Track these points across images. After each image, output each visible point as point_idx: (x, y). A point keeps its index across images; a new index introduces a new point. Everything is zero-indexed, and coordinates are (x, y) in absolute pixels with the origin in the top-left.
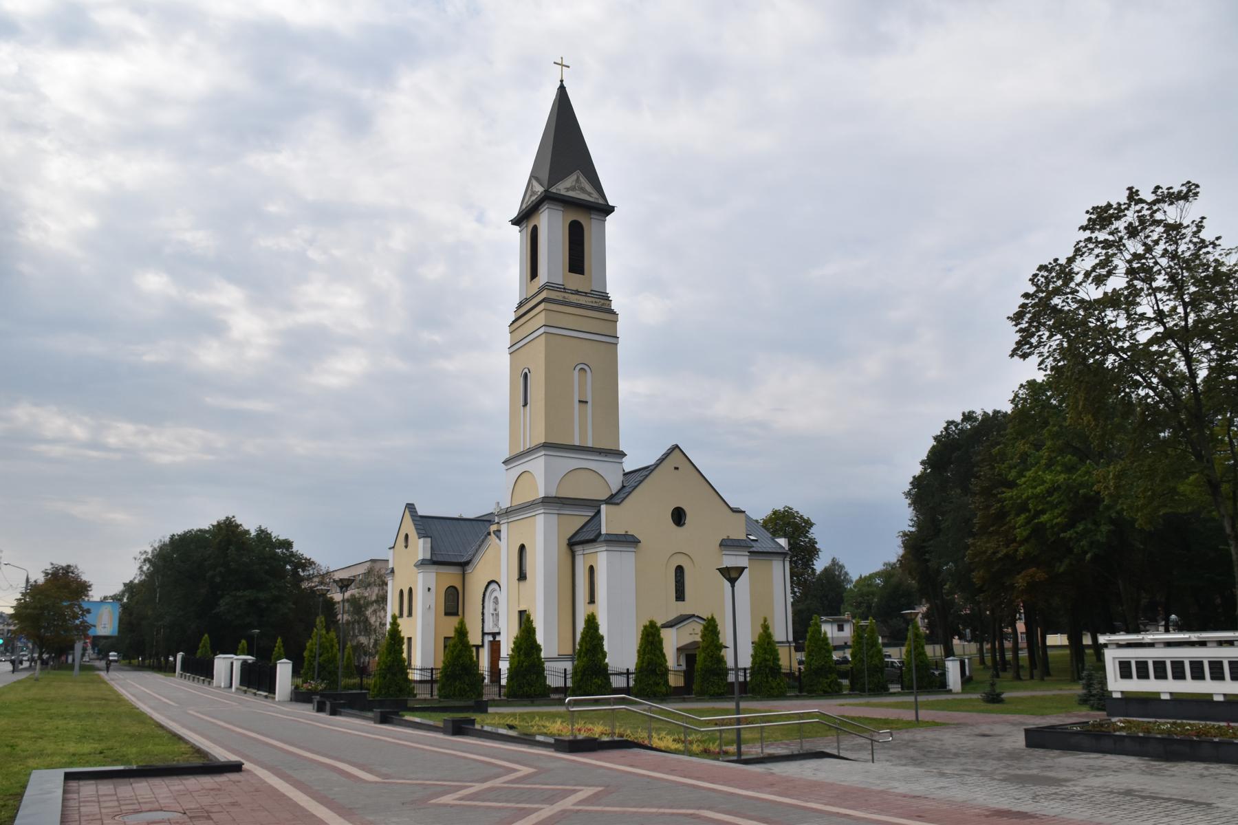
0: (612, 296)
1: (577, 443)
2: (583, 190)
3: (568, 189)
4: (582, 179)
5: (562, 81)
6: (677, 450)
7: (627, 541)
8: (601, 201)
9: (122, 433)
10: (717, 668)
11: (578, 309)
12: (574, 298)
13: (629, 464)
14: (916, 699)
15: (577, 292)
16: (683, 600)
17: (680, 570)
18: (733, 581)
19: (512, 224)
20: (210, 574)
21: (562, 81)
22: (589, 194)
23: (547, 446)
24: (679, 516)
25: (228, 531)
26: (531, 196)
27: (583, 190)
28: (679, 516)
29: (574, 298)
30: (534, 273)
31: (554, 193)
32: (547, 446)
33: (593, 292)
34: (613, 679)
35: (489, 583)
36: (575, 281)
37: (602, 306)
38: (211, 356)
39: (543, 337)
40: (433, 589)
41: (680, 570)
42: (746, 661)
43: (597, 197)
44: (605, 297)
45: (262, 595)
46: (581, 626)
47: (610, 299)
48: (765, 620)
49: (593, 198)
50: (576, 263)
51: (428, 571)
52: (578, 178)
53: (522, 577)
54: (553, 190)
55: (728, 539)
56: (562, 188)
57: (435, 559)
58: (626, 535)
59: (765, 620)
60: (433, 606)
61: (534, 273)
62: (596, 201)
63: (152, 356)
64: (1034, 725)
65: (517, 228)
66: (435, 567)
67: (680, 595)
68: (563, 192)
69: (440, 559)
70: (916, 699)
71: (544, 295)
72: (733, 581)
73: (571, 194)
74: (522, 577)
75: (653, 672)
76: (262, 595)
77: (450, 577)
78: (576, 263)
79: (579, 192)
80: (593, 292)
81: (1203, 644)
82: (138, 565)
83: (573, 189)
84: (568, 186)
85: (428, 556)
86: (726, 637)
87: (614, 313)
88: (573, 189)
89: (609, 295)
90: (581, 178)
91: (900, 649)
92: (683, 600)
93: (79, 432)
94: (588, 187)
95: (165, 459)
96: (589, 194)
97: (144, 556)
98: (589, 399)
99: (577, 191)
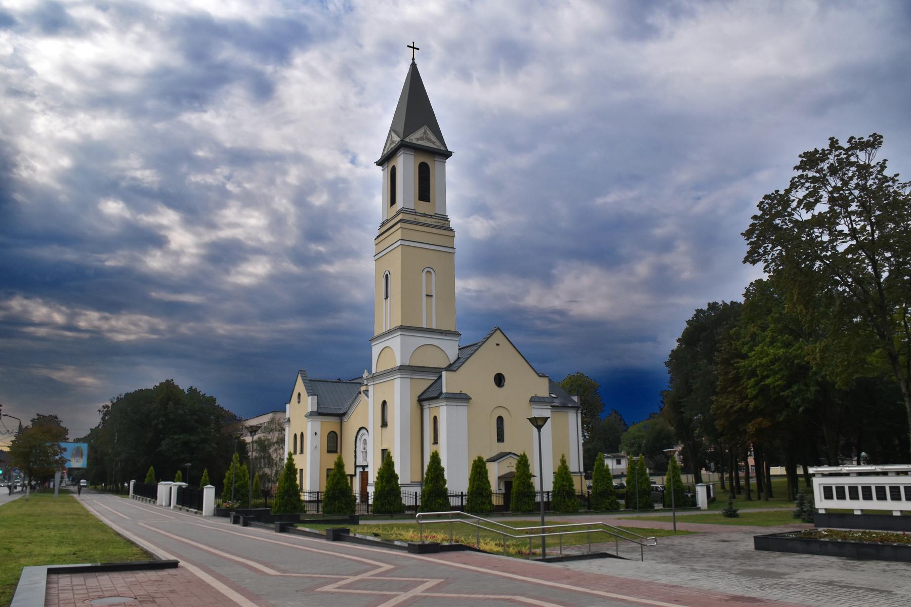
1: (425, 326)
2: (429, 140)
3: (418, 139)
4: (429, 132)
5: (413, 59)
6: (498, 332)
7: (461, 398)
8: (442, 148)
12: (422, 220)
14: (674, 514)
15: (425, 215)
16: (503, 441)
17: (500, 420)
18: (539, 428)
19: (377, 165)
20: (154, 422)
21: (413, 59)
22: (434, 143)
23: (402, 328)
24: (499, 380)
27: (429, 140)
28: (499, 380)
29: (422, 220)
30: (393, 201)
32: (402, 328)
33: (436, 215)
34: (451, 499)
36: (423, 207)
37: (442, 224)
38: (155, 262)
39: (400, 248)
40: (319, 433)
41: (500, 420)
42: (549, 486)
43: (440, 145)
44: (446, 219)
45: (193, 438)
46: (427, 460)
48: (563, 456)
49: (436, 145)
50: (424, 194)
51: (315, 420)
52: (425, 131)
53: (384, 424)
54: (407, 140)
55: (536, 397)
58: (460, 394)
59: (563, 456)
60: (319, 446)
61: (393, 201)
62: (439, 148)
63: (112, 262)
65: (380, 168)
66: (320, 417)
67: (500, 438)
68: (414, 141)
69: (324, 411)
70: (674, 514)
71: (400, 217)
72: (539, 428)
73: (420, 143)
74: (384, 424)
75: (481, 494)
76: (193, 438)
77: (331, 424)
78: (424, 194)
79: (426, 141)
80: (436, 215)
81: (885, 474)
83: (422, 139)
85: (315, 409)
86: (534, 469)
87: (451, 230)
88: (422, 139)
89: (448, 217)
92: (503, 441)
94: (433, 138)
95: (121, 337)
96: (434, 143)
98: (434, 294)
99: (425, 141)
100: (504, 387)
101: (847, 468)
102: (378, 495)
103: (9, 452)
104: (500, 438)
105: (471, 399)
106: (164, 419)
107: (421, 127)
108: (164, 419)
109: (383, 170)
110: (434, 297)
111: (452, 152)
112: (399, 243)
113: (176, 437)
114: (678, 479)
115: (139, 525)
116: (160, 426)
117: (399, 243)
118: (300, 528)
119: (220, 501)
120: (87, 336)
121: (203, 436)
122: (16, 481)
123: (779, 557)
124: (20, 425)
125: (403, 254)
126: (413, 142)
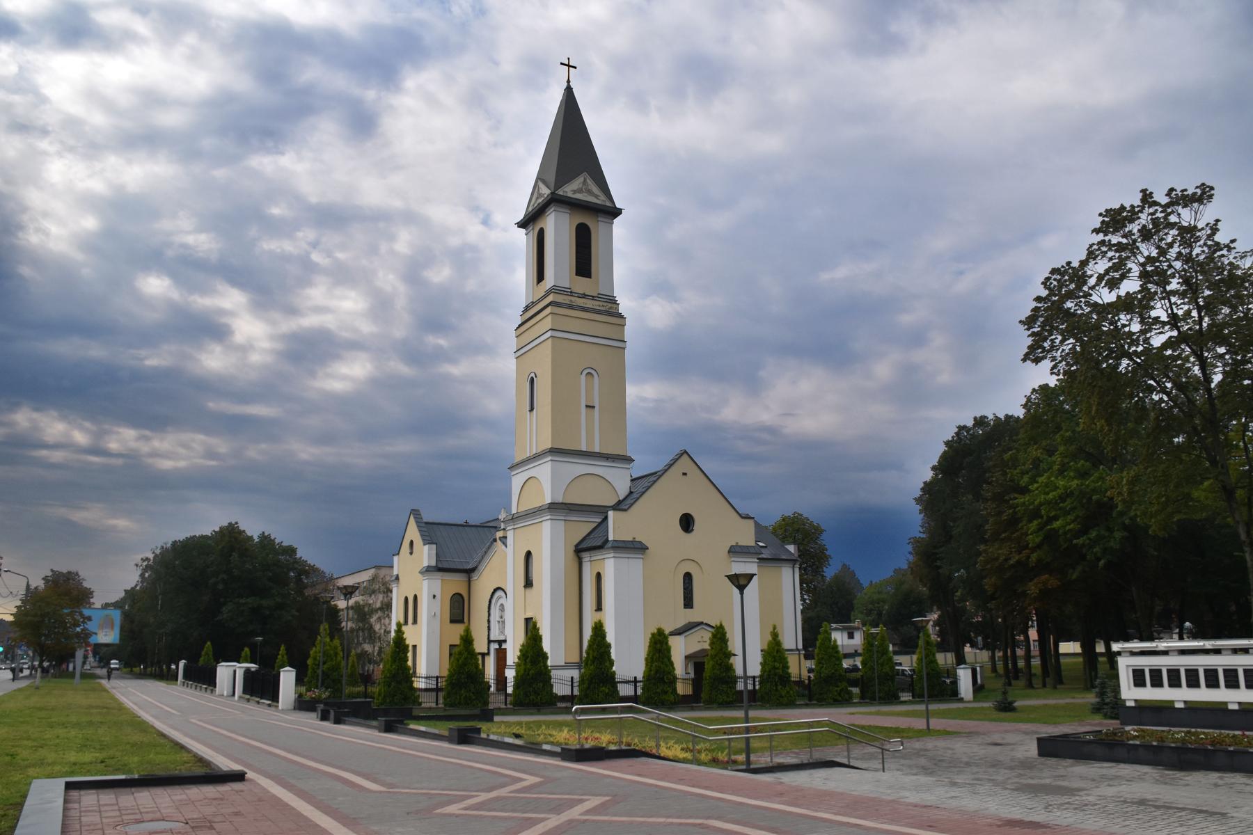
0: (620, 300)
1: (584, 449)
2: (590, 192)
3: (575, 192)
4: (589, 181)
5: (568, 81)
8: (608, 204)
9: (124, 438)
10: (725, 675)
12: (581, 302)
13: (638, 469)
15: (584, 296)
16: (692, 607)
17: (688, 577)
18: (742, 588)
20: (212, 581)
21: (568, 81)
22: (596, 196)
23: (553, 451)
24: (687, 523)
25: (231, 537)
27: (590, 192)
28: (687, 523)
29: (581, 302)
30: (540, 277)
32: (553, 451)
33: (600, 296)
34: (620, 687)
36: (582, 285)
37: (609, 309)
39: (550, 341)
40: (438, 596)
41: (688, 577)
43: (605, 199)
44: (613, 301)
45: (265, 603)
46: (588, 633)
48: (775, 628)
49: (600, 200)
50: (583, 266)
51: (434, 578)
52: (585, 180)
53: (528, 584)
54: (560, 192)
55: (737, 546)
57: (440, 566)
58: (633, 542)
59: (775, 628)
60: (438, 614)
61: (540, 277)
62: (603, 203)
63: (154, 360)
65: (523, 231)
66: (440, 574)
67: (688, 603)
68: (570, 195)
69: (446, 566)
71: (550, 298)
72: (742, 588)
73: (578, 196)
74: (528, 584)
75: (661, 680)
76: (265, 603)
77: (456, 583)
78: (583, 266)
80: (600, 296)
81: (1217, 651)
82: (139, 572)
83: (580, 191)
85: (433, 563)
87: (620, 316)
88: (580, 191)
89: (616, 299)
90: (588, 180)
92: (692, 607)
93: (80, 438)
94: (595, 190)
95: (167, 464)
96: (596, 196)
97: (145, 563)
98: (596, 404)
99: (584, 194)
100: (694, 532)
101: (1165, 644)
102: (520, 681)
103: (12, 622)
104: (688, 603)
106: (225, 576)
108: (225, 576)
110: (597, 409)
111: (621, 209)
112: (549, 334)
113: (243, 601)
115: (191, 722)
116: (221, 587)
117: (549, 334)
119: (303, 689)
120: (120, 461)
121: (279, 600)
122: (22, 661)
123: (1072, 766)
125: (554, 350)
126: (569, 195)
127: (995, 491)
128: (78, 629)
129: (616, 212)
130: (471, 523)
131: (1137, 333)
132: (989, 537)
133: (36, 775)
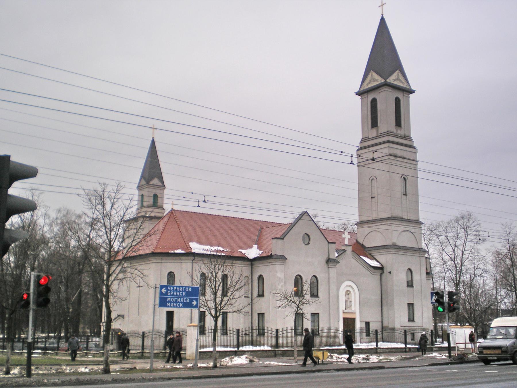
2: (401, 81)
5: (382, 15)
8: (408, 87)
11: (156, 145)
14: (377, 345)
21: (382, 15)
22: (368, 84)
26: (370, 82)
27: (370, 82)
30: (374, 124)
31: (388, 82)
35: (309, 243)
47: (413, 140)
49: (404, 85)
52: (398, 73)
56: (391, 80)
61: (374, 124)
64: (475, 387)
68: (392, 82)
70: (377, 345)
83: (395, 80)
84: (394, 78)
89: (412, 138)
91: (192, 310)
94: (403, 80)
96: (403, 83)
105: (287, 259)
107: (369, 73)
109: (361, 99)
111: (415, 91)
114: (101, 286)
118: (491, 363)
124: (272, 253)
127: (480, 280)
128: (12, 265)
129: (412, 92)
130: (330, 229)
131: (44, 285)
132: (305, 333)
133: (95, 297)
